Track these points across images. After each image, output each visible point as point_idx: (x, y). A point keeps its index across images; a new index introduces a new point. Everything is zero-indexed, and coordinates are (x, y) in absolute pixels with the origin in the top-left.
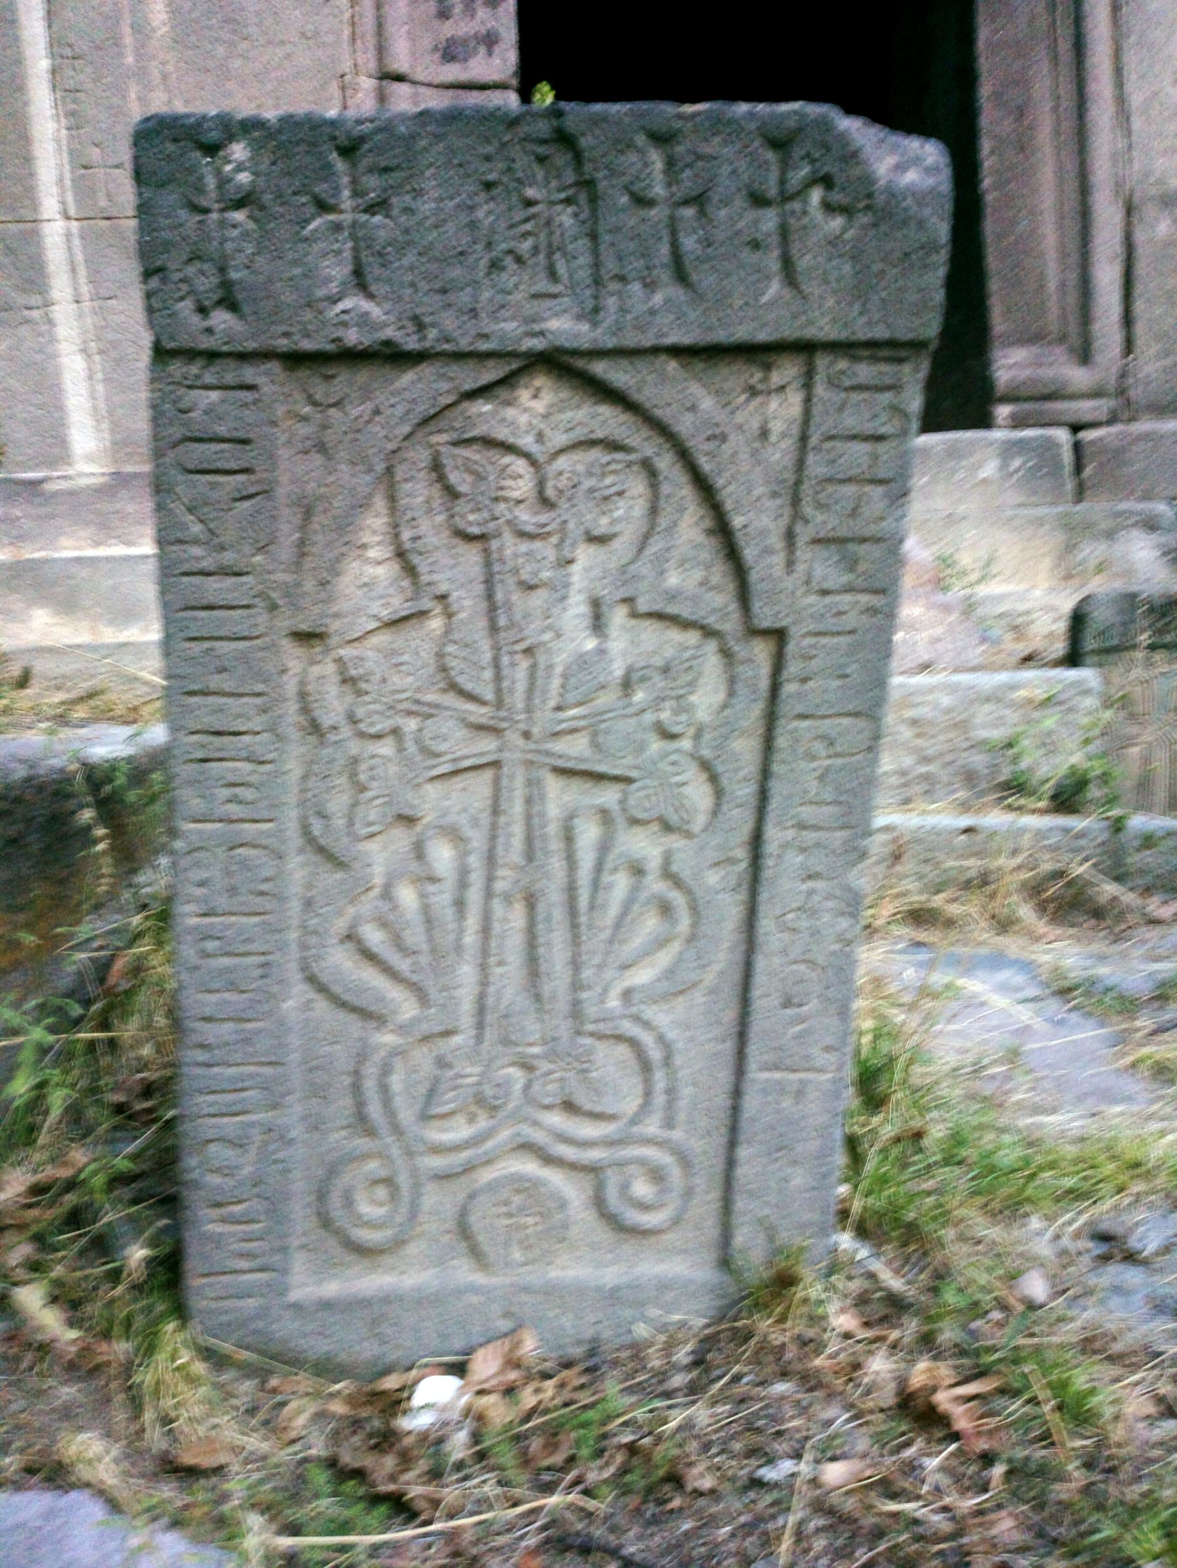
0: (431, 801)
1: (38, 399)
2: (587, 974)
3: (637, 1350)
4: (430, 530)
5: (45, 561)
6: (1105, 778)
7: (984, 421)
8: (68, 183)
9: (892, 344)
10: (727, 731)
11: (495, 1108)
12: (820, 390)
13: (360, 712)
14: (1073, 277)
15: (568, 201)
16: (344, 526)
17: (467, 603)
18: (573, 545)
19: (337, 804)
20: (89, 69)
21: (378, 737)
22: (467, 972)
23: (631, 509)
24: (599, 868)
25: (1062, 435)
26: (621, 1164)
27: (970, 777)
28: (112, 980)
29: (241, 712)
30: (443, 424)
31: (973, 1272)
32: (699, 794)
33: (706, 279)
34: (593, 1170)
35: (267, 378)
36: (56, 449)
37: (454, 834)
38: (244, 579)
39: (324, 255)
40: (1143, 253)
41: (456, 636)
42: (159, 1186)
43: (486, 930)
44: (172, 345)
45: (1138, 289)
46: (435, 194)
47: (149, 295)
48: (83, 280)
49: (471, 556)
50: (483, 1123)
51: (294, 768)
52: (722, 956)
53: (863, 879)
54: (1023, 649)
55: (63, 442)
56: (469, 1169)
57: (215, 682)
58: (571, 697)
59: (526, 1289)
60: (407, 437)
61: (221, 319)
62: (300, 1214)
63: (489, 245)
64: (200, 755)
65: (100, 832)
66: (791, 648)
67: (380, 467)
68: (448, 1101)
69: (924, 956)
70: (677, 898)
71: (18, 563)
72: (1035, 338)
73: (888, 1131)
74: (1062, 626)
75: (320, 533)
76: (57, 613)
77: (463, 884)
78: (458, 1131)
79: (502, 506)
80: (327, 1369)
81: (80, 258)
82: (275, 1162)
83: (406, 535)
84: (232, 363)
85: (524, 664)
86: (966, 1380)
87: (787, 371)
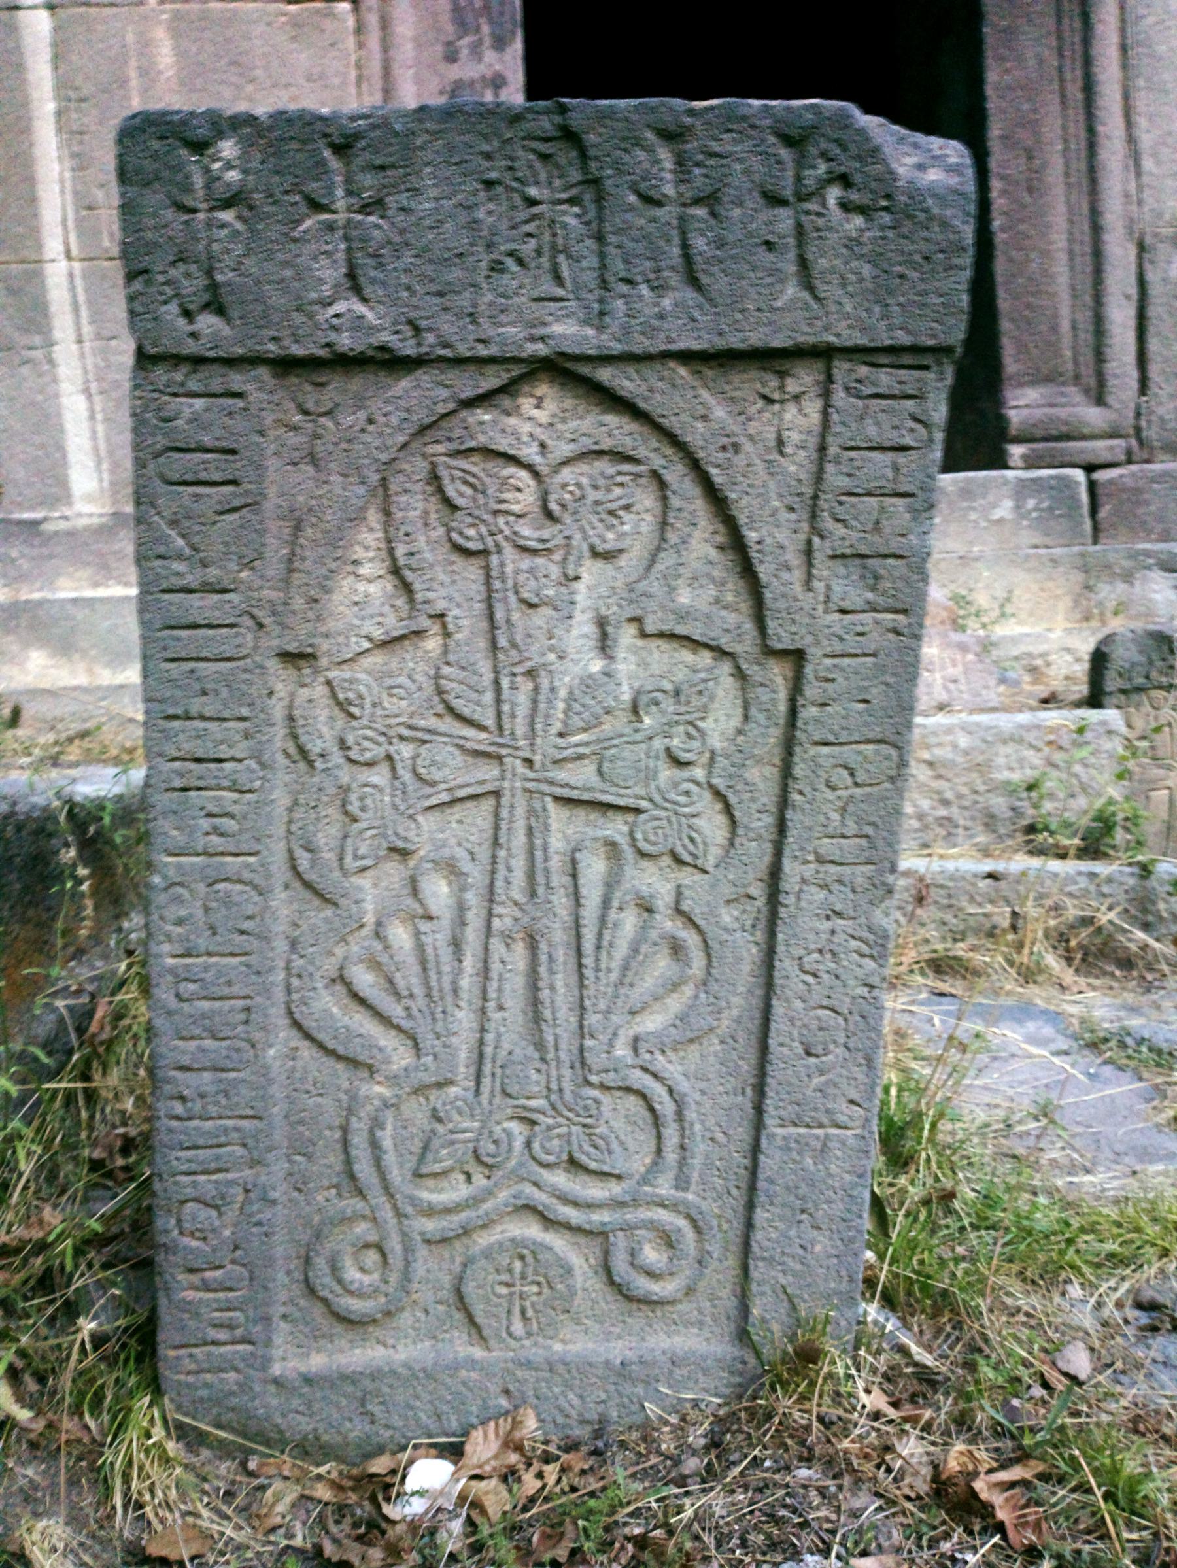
0: (426, 832)
1: (37, 439)
2: (592, 1019)
3: (647, 1433)
4: (426, 545)
5: (40, 603)
6: (1132, 821)
7: (999, 461)
8: (71, 224)
9: (915, 349)
10: (742, 756)
11: (490, 1167)
12: (839, 397)
13: (350, 740)
14: (1085, 317)
15: (571, 201)
16: (336, 541)
17: (465, 622)
18: (578, 564)
19: (326, 836)
20: (94, 112)
21: (370, 764)
22: (464, 1018)
23: (637, 527)
24: (606, 903)
25: (1079, 475)
26: (628, 1228)
27: (990, 821)
28: (93, 1028)
29: (224, 737)
30: (438, 434)
31: (1009, 1343)
32: (712, 826)
33: (717, 282)
34: (601, 1234)
35: (255, 384)
36: (57, 490)
37: (451, 869)
38: (227, 596)
39: (315, 258)
40: (1156, 290)
41: (451, 658)
42: (132, 1251)
43: (485, 971)
44: (154, 351)
45: (1151, 330)
46: (433, 193)
47: (131, 299)
48: (84, 321)
49: (472, 571)
50: (480, 1181)
51: (281, 798)
52: (739, 1001)
53: (889, 917)
54: (1043, 691)
55: (63, 483)
56: (466, 1232)
57: (196, 705)
58: (577, 722)
59: (528, 1364)
60: (405, 446)
61: (207, 322)
62: (283, 1284)
63: (490, 246)
64: (177, 783)
65: (82, 871)
66: (809, 670)
67: (375, 478)
68: (444, 1158)
69: (948, 1005)
70: (691, 939)
71: (15, 604)
72: (1050, 379)
73: (915, 1193)
74: (1082, 669)
75: (310, 546)
76: (53, 655)
77: (461, 921)
78: (455, 1191)
79: (501, 521)
80: (310, 1449)
81: (82, 298)
82: (259, 1224)
83: (401, 550)
84: (216, 368)
85: (526, 686)
86: (1003, 1466)
87: (804, 378)
